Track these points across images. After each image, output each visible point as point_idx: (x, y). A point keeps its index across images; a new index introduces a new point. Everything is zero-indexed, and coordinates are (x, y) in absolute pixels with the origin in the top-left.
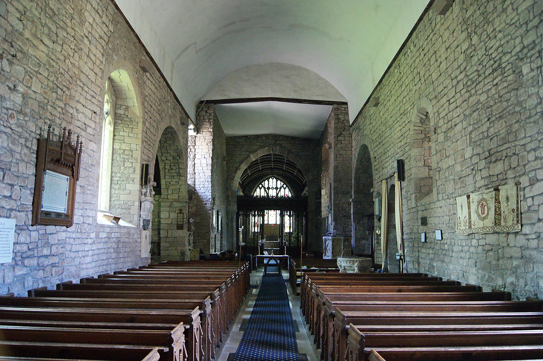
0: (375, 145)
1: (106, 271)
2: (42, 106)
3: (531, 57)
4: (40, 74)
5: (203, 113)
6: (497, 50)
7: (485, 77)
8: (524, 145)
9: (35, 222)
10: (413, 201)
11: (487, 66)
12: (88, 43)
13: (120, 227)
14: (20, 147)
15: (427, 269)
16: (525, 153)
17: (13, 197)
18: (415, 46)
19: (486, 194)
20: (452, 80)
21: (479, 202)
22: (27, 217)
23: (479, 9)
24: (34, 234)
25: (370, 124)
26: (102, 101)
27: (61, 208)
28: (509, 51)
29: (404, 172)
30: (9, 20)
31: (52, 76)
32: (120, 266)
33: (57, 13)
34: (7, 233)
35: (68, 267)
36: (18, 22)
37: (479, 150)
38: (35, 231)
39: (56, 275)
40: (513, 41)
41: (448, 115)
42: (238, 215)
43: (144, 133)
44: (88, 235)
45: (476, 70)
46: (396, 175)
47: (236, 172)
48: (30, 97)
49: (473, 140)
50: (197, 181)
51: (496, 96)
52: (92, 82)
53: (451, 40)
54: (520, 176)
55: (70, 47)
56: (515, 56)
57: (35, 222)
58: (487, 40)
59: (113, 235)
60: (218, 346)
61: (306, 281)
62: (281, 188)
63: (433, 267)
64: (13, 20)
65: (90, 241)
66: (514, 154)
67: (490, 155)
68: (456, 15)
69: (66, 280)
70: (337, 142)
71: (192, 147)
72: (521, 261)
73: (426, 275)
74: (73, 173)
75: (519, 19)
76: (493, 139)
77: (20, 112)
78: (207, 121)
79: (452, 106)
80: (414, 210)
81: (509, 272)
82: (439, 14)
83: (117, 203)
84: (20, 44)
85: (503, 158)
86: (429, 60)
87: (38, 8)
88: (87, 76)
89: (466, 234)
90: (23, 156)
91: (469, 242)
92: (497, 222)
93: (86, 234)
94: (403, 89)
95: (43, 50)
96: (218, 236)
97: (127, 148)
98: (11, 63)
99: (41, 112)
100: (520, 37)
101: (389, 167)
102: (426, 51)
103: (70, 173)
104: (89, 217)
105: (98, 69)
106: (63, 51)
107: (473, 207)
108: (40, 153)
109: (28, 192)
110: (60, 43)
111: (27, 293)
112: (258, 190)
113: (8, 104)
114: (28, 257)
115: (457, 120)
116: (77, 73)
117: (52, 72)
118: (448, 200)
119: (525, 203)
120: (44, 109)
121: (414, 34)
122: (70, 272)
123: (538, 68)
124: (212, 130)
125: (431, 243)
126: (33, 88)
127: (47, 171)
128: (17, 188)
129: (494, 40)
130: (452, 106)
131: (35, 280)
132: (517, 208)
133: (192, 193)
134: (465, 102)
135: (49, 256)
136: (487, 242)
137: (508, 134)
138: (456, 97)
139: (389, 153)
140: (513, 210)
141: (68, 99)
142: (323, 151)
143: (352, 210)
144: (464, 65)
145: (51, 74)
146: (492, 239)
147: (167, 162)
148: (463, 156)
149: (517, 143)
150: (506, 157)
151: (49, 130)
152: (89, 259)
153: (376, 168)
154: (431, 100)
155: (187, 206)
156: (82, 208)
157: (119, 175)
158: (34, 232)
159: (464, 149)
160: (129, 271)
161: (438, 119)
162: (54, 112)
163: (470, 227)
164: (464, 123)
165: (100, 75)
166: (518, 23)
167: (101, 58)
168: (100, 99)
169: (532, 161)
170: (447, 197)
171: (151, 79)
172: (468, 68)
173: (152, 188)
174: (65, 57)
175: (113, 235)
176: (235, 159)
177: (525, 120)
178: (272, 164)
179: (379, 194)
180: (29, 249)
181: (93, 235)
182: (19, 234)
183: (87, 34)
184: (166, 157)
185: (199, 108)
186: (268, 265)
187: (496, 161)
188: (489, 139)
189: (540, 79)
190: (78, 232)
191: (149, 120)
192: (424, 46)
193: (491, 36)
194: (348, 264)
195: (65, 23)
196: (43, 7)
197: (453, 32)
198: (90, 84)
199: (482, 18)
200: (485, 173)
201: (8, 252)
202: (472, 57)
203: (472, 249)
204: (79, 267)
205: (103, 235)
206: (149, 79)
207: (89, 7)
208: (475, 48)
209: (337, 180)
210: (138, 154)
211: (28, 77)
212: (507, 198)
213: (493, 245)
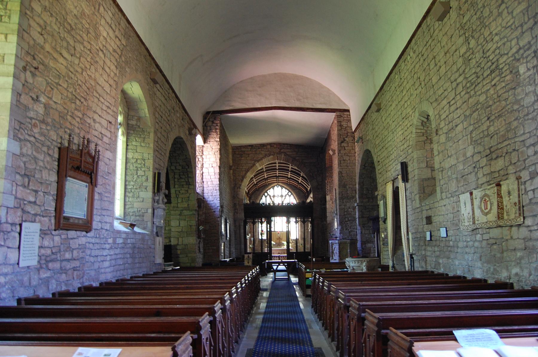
1: (123, 275)
3: (527, 57)
4: (60, 85)
6: (494, 52)
7: (484, 79)
8: (523, 141)
9: (58, 227)
10: (418, 201)
11: (485, 68)
12: (102, 56)
13: (135, 233)
14: (43, 155)
15: (433, 266)
16: (525, 149)
17: (38, 202)
18: (414, 52)
19: (489, 189)
20: (452, 83)
21: (482, 199)
22: (49, 222)
23: (476, 14)
24: (57, 238)
25: (373, 129)
26: (116, 111)
28: (506, 52)
29: (407, 173)
30: (31, 34)
31: (70, 88)
32: (136, 271)
33: (74, 27)
34: (32, 237)
35: (88, 271)
36: (39, 35)
37: (480, 148)
39: (77, 278)
40: (509, 43)
41: (449, 116)
43: (156, 143)
45: (475, 73)
46: (400, 177)
47: (242, 181)
48: (52, 108)
49: (474, 139)
50: (205, 189)
51: (495, 96)
52: (107, 93)
53: (450, 45)
54: (520, 171)
55: (86, 59)
56: (512, 57)
57: (58, 227)
58: (484, 43)
59: (129, 241)
60: (237, 342)
61: (317, 281)
62: (285, 196)
63: (439, 264)
66: (514, 150)
67: (491, 153)
68: (453, 21)
69: (87, 284)
71: (199, 157)
72: (524, 252)
73: (432, 272)
74: (92, 180)
75: (514, 22)
76: (493, 137)
77: (43, 122)
79: (452, 108)
80: (419, 210)
81: (513, 264)
83: (131, 210)
84: (42, 57)
85: (504, 155)
86: (429, 65)
87: (57, 23)
88: (103, 88)
89: (470, 229)
90: (46, 164)
91: (473, 238)
92: (500, 216)
93: (104, 239)
94: (403, 94)
95: (63, 63)
97: (139, 157)
98: (33, 75)
99: (61, 122)
100: (516, 40)
101: (393, 170)
102: (425, 56)
103: (89, 180)
104: (106, 222)
105: (112, 80)
106: (80, 64)
107: (477, 203)
108: (61, 161)
109: (51, 198)
110: (78, 56)
112: (264, 198)
113: (32, 114)
114: (51, 261)
115: (458, 121)
116: (93, 85)
118: (452, 199)
119: (526, 196)
121: (413, 41)
122: (90, 276)
123: (534, 67)
124: (218, 140)
126: (54, 99)
127: (68, 178)
128: (41, 193)
129: (492, 43)
130: (452, 108)
132: (519, 201)
133: (201, 201)
134: (465, 104)
135: (71, 260)
136: (491, 236)
137: (508, 131)
138: (456, 99)
140: (515, 204)
141: (85, 110)
142: (326, 157)
143: (357, 214)
144: (463, 67)
145: (70, 85)
146: (495, 233)
148: (465, 155)
149: (517, 140)
150: (507, 153)
151: (70, 139)
152: (107, 264)
153: (379, 172)
154: (431, 103)
155: (196, 214)
157: (132, 183)
158: (57, 237)
160: (144, 276)
161: (439, 121)
162: (74, 122)
163: (474, 223)
164: (465, 123)
165: (115, 87)
168: (115, 109)
169: (532, 156)
170: (450, 195)
171: (161, 90)
172: (466, 71)
173: (164, 196)
174: (82, 69)
175: (129, 241)
176: (241, 167)
178: (277, 173)
179: (384, 197)
180: (53, 253)
181: (110, 241)
182: (43, 238)
183: (101, 48)
184: (175, 167)
185: (206, 118)
186: (277, 271)
187: (497, 157)
188: (490, 137)
189: (537, 78)
191: (160, 130)
194: (357, 264)
195: (81, 37)
198: (106, 95)
200: (486, 170)
201: (33, 255)
202: (470, 60)
203: (476, 244)
204: (98, 271)
205: (120, 241)
207: (103, 22)
209: (342, 185)
210: (150, 163)
211: (49, 88)
212: (509, 193)
213: (496, 239)
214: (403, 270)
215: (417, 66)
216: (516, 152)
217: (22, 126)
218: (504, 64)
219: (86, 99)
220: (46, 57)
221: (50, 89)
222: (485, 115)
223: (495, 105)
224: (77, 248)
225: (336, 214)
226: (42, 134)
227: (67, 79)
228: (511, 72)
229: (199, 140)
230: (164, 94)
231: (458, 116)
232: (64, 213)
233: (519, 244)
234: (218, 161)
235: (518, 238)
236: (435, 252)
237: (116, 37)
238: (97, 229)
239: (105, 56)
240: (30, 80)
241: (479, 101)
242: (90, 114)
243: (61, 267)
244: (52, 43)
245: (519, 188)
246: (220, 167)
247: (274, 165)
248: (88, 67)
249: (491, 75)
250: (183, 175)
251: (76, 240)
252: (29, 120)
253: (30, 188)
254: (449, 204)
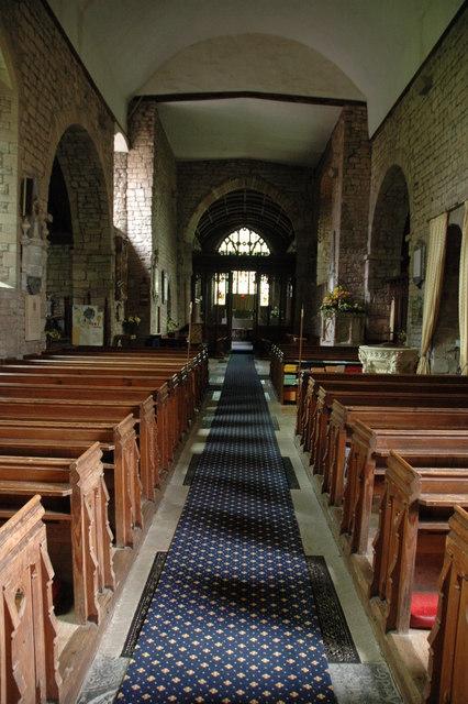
5: (139, 117)
25: (410, 128)
42: (194, 281)
43: (23, 124)
70: (348, 166)
96: (164, 309)
133: (123, 243)
147: (80, 190)
173: (45, 225)
185: (133, 108)
214: (453, 372)
225: (334, 271)
229: (120, 143)
234: (151, 178)
246: (153, 189)
250: (92, 197)
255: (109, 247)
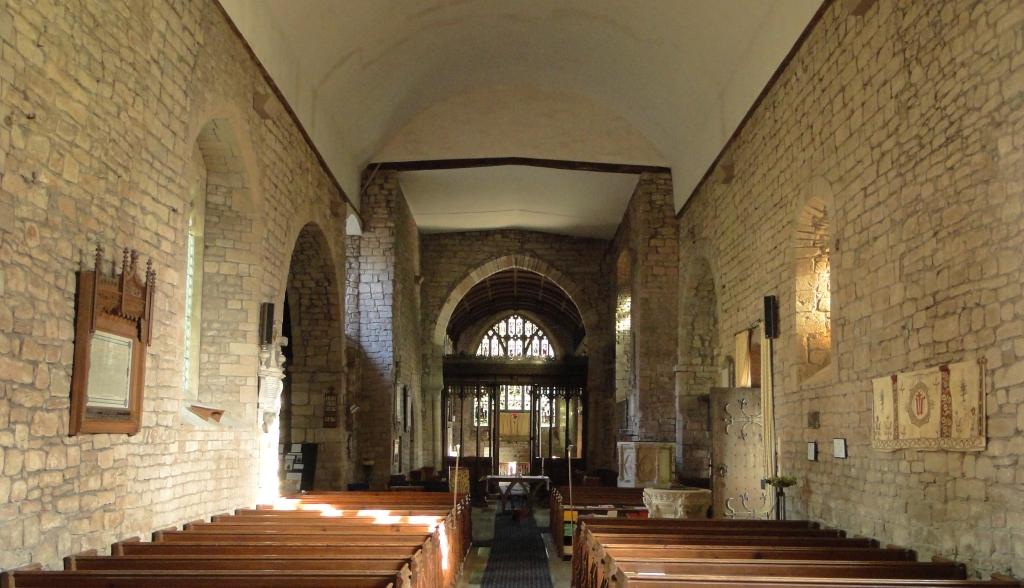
0: (725, 260)
1: (198, 515)
2: (81, 209)
4: (77, 146)
6: (955, 101)
7: (933, 152)
8: (995, 290)
11: (937, 131)
14: (46, 291)
15: (818, 512)
16: (997, 305)
18: (805, 70)
20: (872, 149)
21: (913, 391)
22: (56, 421)
23: (927, 13)
24: (73, 452)
27: (119, 400)
28: (977, 105)
31: (97, 148)
33: (100, 20)
35: (130, 511)
36: (33, 48)
37: (915, 291)
38: (75, 445)
39: (110, 526)
41: (864, 216)
44: (166, 448)
46: (762, 325)
47: (440, 307)
49: (906, 271)
50: (364, 328)
51: (951, 191)
52: (168, 150)
54: (986, 348)
55: (126, 85)
56: (987, 116)
57: (75, 428)
63: (829, 510)
64: (26, 47)
65: (168, 459)
66: (978, 305)
67: (936, 303)
69: (128, 536)
73: (817, 525)
74: (139, 332)
75: (997, 47)
77: (45, 224)
78: (384, 204)
79: (871, 201)
80: (796, 397)
81: (964, 525)
82: (853, 14)
88: (159, 140)
90: (52, 307)
92: (945, 432)
93: (163, 446)
94: (778, 156)
95: (81, 99)
98: (26, 132)
99: (81, 219)
102: (825, 83)
103: (134, 332)
104: (166, 412)
108: (80, 300)
111: (61, 563)
112: (485, 340)
113: (23, 211)
114: (64, 495)
116: (141, 136)
117: (97, 140)
118: (858, 383)
119: (994, 399)
120: (86, 214)
121: (805, 45)
125: (826, 462)
126: (66, 176)
127: (97, 332)
128: (43, 367)
130: (871, 201)
131: (76, 540)
132: (980, 407)
133: (357, 355)
134: (895, 196)
135: (99, 491)
136: (927, 468)
137: (969, 266)
139: (750, 281)
140: (973, 410)
142: (619, 265)
145: (95, 144)
146: (934, 462)
148: (887, 300)
149: (984, 285)
150: (964, 309)
153: (725, 308)
154: (831, 184)
156: (154, 396)
159: (888, 287)
162: (104, 218)
163: (896, 437)
164: (892, 236)
165: (182, 134)
166: (995, 52)
167: (182, 101)
170: (855, 377)
173: (280, 349)
174: (119, 107)
175: (209, 446)
177: (999, 243)
180: (65, 480)
182: (47, 453)
183: (156, 56)
188: (936, 271)
190: (147, 443)
191: (272, 214)
192: (822, 73)
193: (946, 70)
196: (77, 14)
197: (878, 53)
199: (932, 35)
200: (925, 337)
202: (909, 108)
203: (900, 479)
204: (149, 510)
206: (271, 131)
208: (917, 91)
211: (56, 156)
212: (963, 388)
215: (810, 100)
216: (981, 309)
217: (7, 236)
218: (971, 129)
219: (126, 169)
220: (47, 92)
221: (59, 156)
222: (929, 226)
223: (949, 210)
224: (112, 468)
226: (44, 248)
227: (89, 131)
228: (984, 147)
229: (353, 225)
230: (281, 138)
231: (878, 220)
232: (88, 401)
233: (976, 490)
234: (391, 269)
235: (975, 478)
236: (822, 484)
237: (185, 28)
238: (149, 427)
239: (162, 73)
240: (20, 143)
241: (920, 195)
242: (135, 197)
243: (80, 507)
244: (59, 60)
245: (981, 381)
247: (508, 275)
248: (130, 101)
249: (947, 146)
250: (320, 299)
251: (109, 452)
252: (18, 224)
253: (24, 358)
254: (853, 393)
255: (340, 362)
